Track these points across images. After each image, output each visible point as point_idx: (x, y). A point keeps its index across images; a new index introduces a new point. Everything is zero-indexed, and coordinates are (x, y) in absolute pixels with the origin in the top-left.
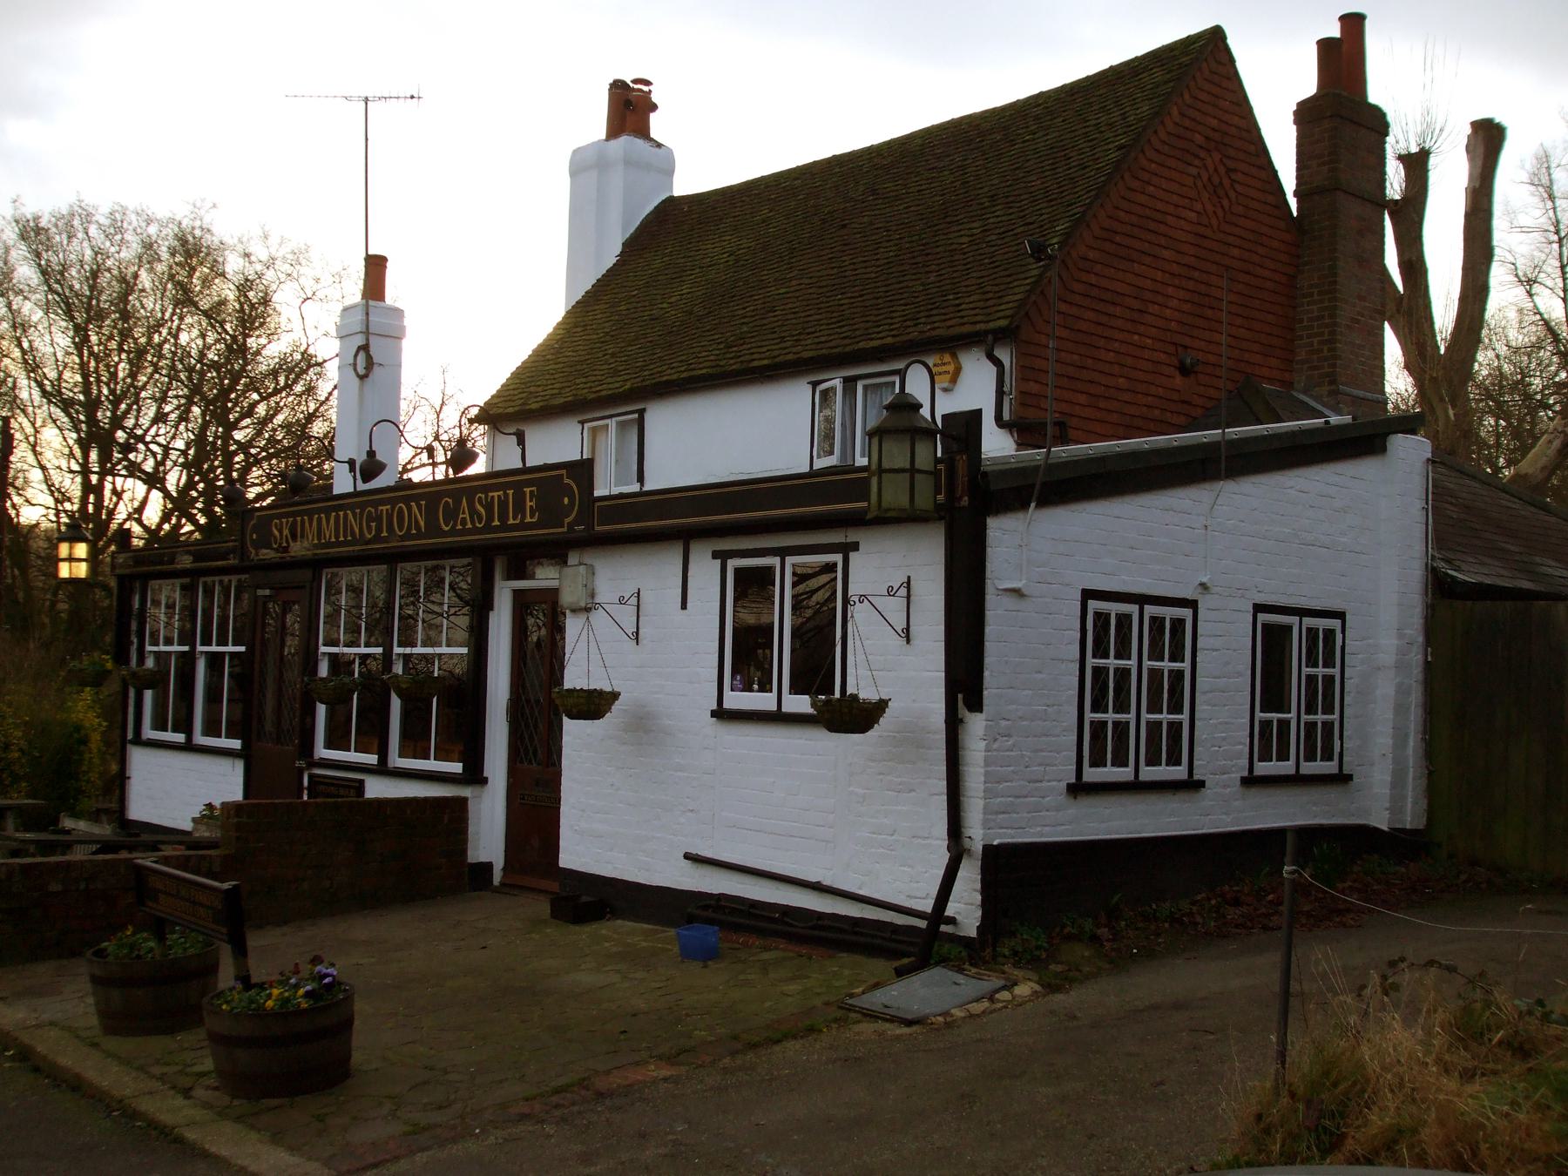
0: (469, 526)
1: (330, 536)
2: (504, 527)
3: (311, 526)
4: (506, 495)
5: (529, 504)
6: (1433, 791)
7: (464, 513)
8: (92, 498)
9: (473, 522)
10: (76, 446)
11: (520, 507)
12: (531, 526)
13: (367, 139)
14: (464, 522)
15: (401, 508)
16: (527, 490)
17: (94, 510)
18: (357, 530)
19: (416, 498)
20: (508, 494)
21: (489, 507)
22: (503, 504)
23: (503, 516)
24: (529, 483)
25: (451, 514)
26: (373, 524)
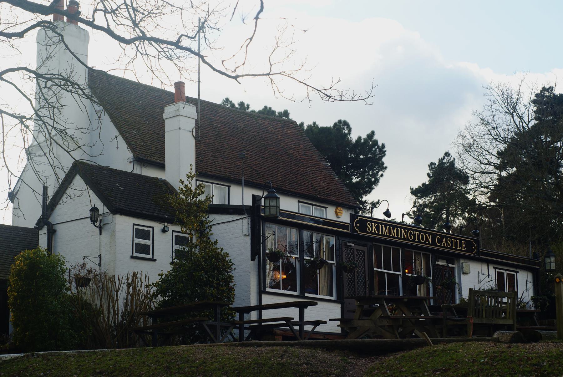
0: (446, 246)
1: (395, 234)
2: (456, 249)
3: (386, 229)
4: (457, 241)
5: (463, 245)
6: (534, 294)
7: (444, 242)
8: (284, 322)
9: (447, 245)
10: (168, 46)
11: (461, 245)
12: (463, 251)
13: (77, 220)
14: (444, 244)
15: (422, 234)
16: (463, 242)
17: (308, 332)
18: (406, 236)
19: (404, 229)
20: (398, 230)
21: (452, 242)
22: (456, 243)
23: (456, 246)
24: (464, 240)
25: (440, 241)
26: (412, 236)
